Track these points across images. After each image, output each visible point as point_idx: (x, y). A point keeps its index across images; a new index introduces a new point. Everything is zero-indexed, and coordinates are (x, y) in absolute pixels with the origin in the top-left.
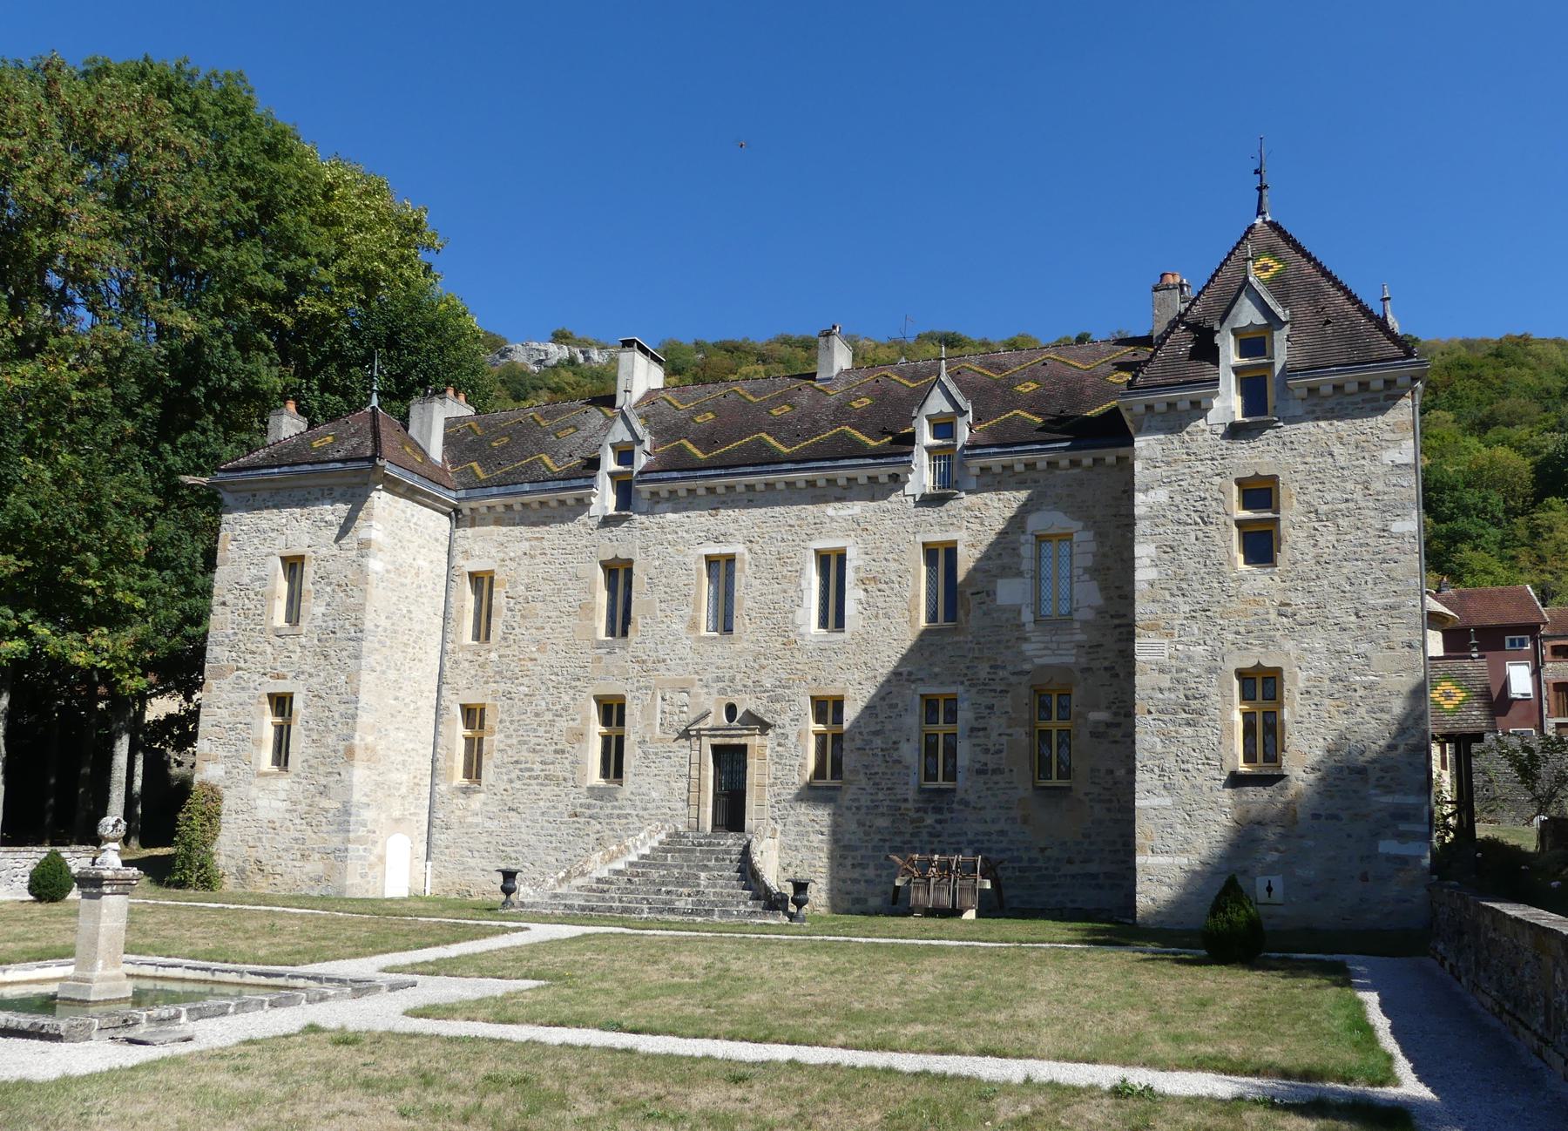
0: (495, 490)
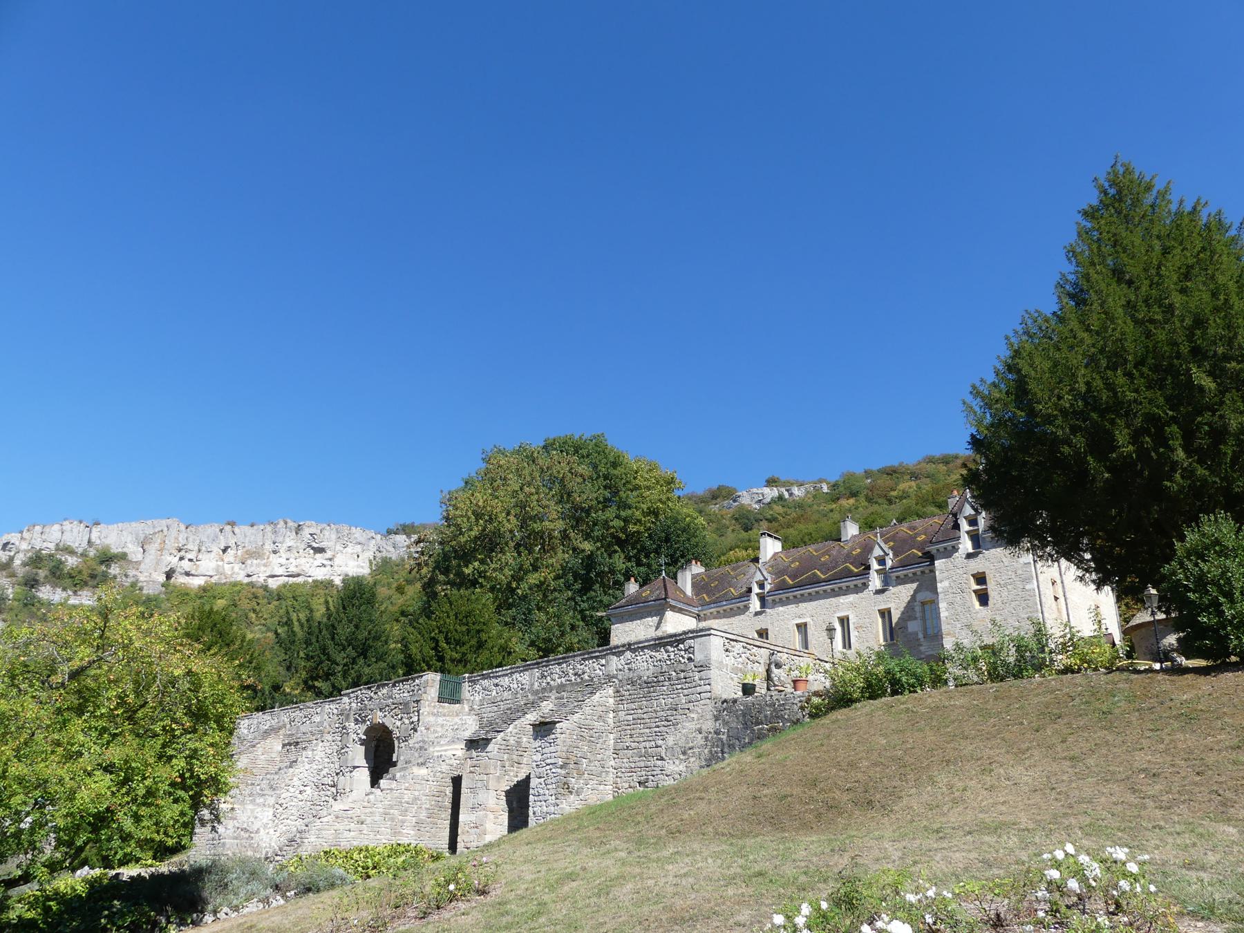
0: (712, 605)
